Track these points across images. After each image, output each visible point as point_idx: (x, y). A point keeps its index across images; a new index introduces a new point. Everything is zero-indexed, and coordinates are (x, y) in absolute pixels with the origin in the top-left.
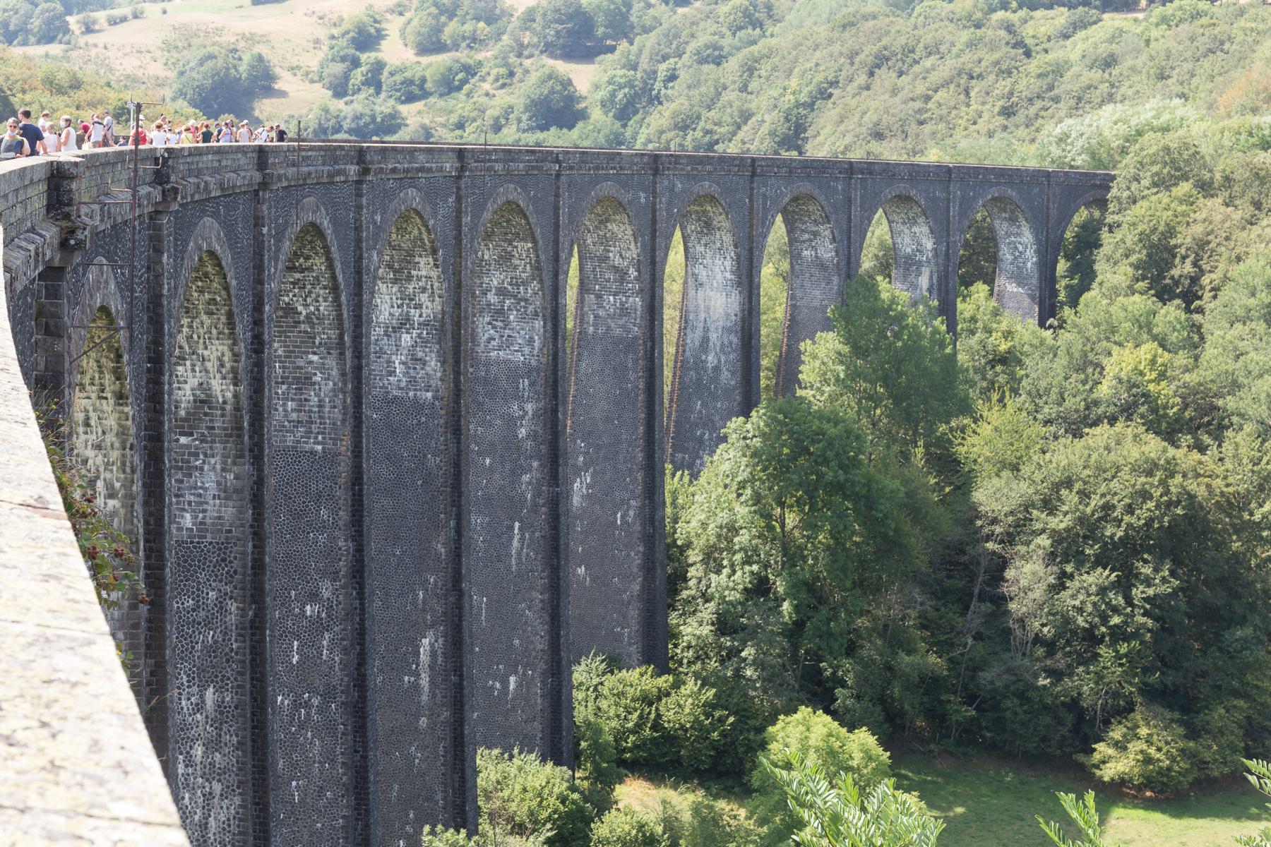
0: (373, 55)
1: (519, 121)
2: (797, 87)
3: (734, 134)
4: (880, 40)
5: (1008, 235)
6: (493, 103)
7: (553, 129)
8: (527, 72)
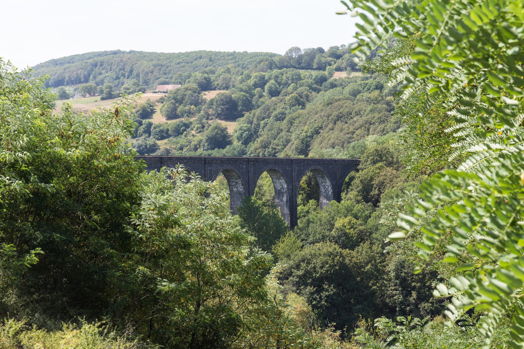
0: (147, 120)
1: (204, 146)
2: (307, 129)
3: (283, 149)
4: (339, 110)
5: (322, 183)
6: (195, 139)
7: (216, 149)
8: (210, 125)
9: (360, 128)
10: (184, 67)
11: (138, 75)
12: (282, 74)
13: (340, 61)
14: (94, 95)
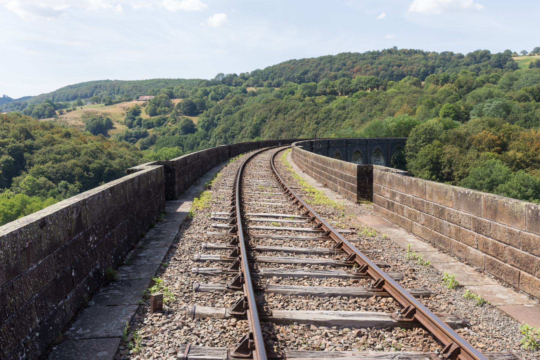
1: (180, 132)
3: (240, 133)
7: (189, 134)
11: (123, 93)
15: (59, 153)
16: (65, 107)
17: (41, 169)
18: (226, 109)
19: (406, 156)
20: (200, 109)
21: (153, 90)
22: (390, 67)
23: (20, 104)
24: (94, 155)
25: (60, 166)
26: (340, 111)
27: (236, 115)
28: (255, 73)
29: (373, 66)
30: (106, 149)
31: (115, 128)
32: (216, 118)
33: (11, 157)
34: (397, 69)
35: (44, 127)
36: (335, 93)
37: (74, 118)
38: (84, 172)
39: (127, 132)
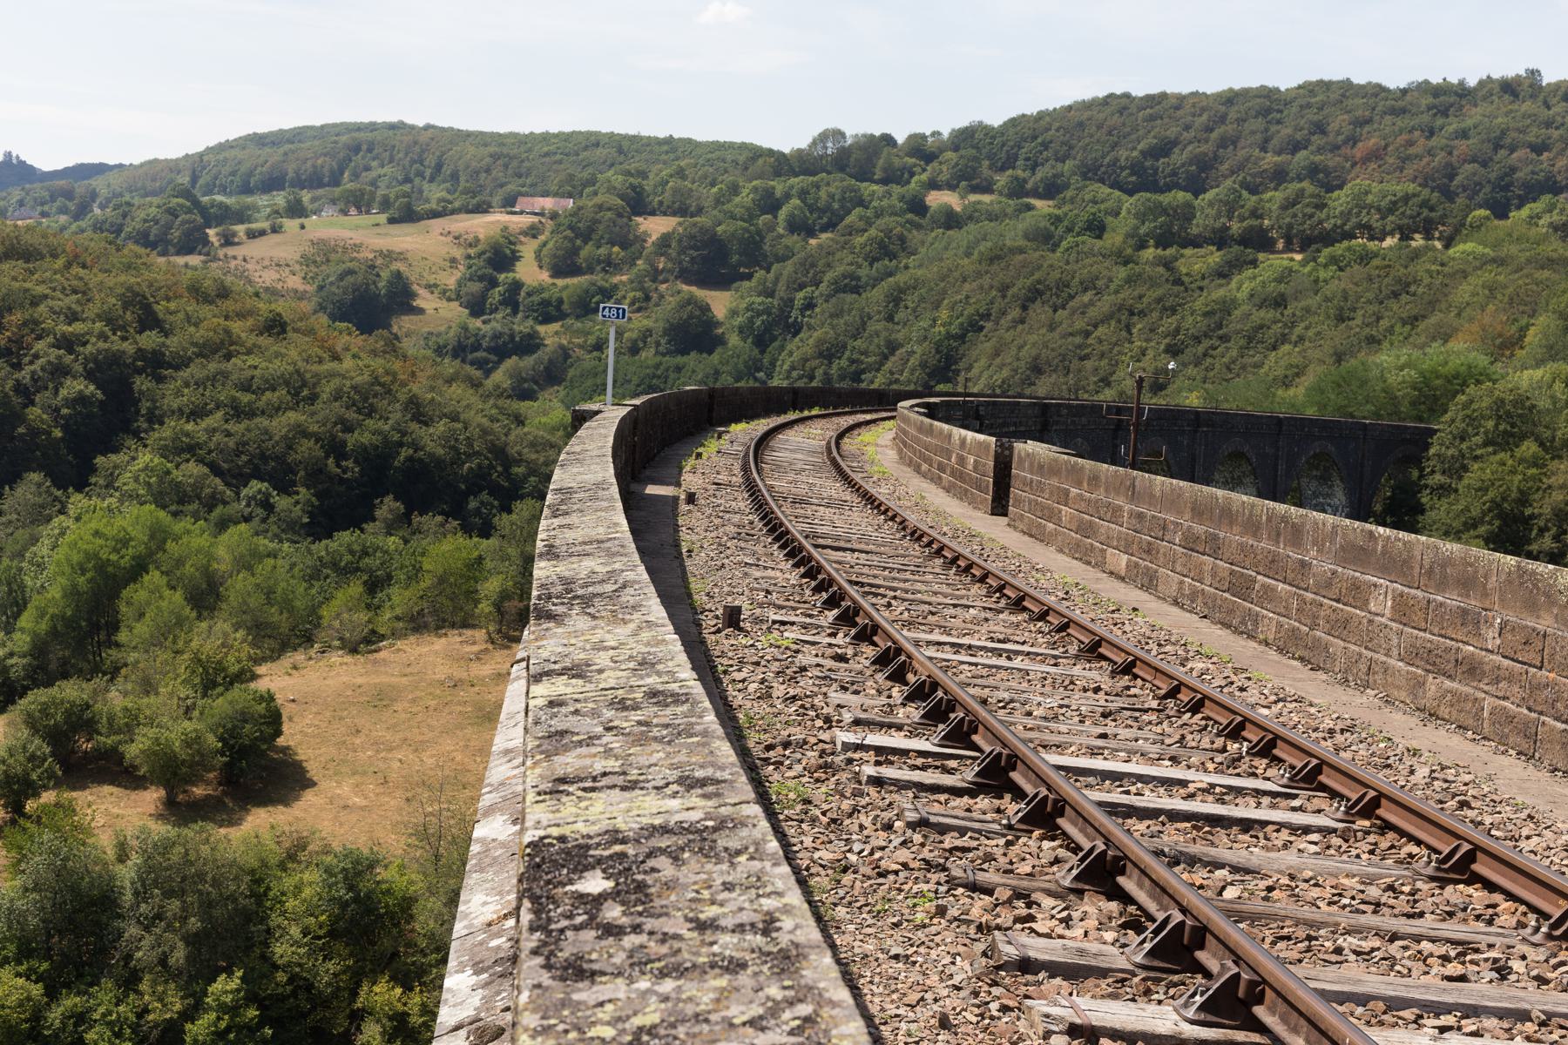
1: (658, 344)
3: (882, 364)
7: (693, 354)
9: (1102, 322)
10: (560, 162)
11: (455, 177)
12: (818, 188)
13: (935, 164)
14: (368, 212)
15: (246, 387)
16: (241, 216)
17: (187, 435)
18: (840, 269)
19: (1426, 486)
20: (740, 264)
21: (571, 177)
22: (1503, 153)
23: (75, 187)
24: (365, 400)
25: (248, 430)
26: (1262, 313)
27: (876, 296)
28: (968, 137)
29: (1434, 142)
30: (404, 384)
31: (421, 311)
32: (798, 303)
33: (92, 387)
34: (1528, 162)
35: (197, 290)
36: (1259, 241)
37: (271, 259)
38: (327, 457)
39: (465, 328)
